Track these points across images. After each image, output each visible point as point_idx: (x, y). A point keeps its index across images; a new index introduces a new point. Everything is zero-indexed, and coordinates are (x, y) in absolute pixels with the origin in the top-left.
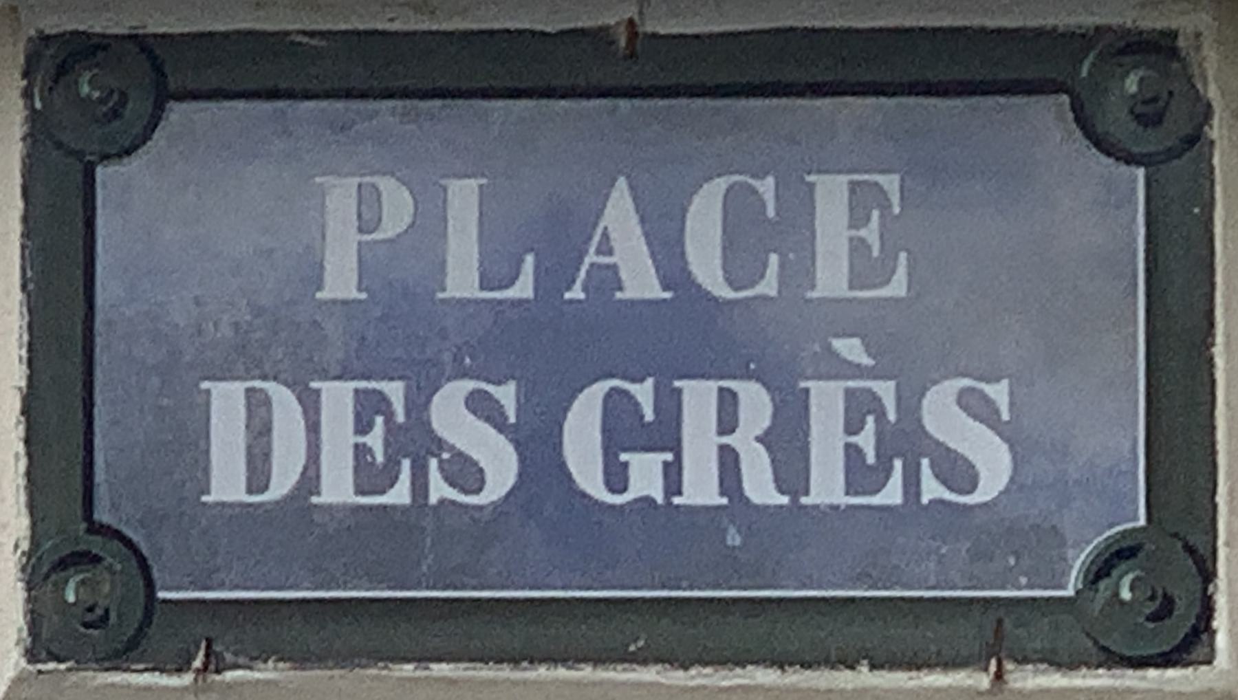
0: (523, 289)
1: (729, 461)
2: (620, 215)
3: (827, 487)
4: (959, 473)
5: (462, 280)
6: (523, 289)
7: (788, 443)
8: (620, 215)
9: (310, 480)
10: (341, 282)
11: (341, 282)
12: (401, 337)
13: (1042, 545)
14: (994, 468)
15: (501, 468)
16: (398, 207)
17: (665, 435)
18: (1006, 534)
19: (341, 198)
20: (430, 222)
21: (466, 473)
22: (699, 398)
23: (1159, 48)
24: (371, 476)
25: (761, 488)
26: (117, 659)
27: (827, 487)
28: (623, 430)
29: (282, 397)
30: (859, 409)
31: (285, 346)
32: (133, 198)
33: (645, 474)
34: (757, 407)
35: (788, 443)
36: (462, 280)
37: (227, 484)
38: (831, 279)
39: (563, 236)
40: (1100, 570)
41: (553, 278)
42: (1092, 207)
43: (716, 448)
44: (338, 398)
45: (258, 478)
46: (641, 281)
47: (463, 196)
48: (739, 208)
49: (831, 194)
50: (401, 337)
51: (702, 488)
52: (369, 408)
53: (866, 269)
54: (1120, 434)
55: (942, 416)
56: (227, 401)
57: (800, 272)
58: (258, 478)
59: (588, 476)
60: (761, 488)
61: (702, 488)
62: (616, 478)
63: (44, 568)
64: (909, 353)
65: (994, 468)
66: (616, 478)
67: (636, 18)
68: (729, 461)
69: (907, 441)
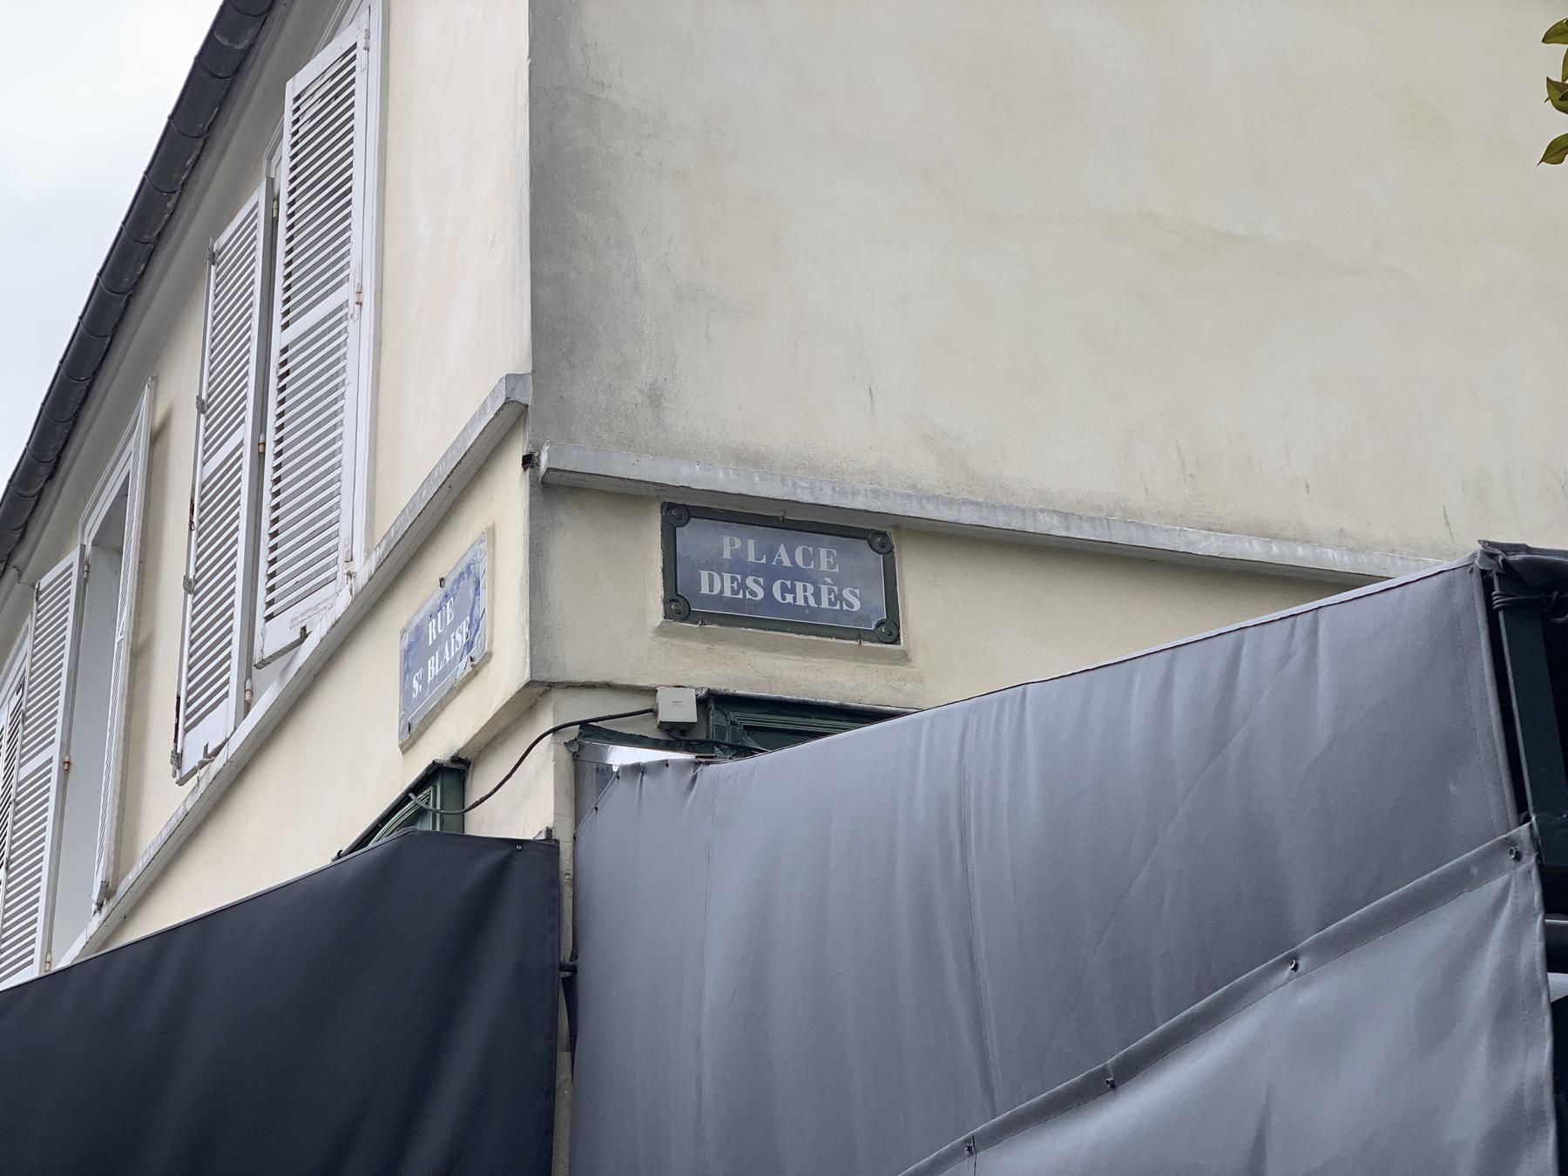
0: (764, 561)
1: (806, 598)
2: (782, 550)
3: (825, 604)
4: (850, 605)
5: (751, 558)
6: (764, 561)
7: (817, 595)
8: (782, 550)
9: (722, 591)
10: (727, 555)
11: (727, 555)
12: (739, 567)
13: (868, 620)
14: (857, 606)
15: (761, 594)
16: (738, 544)
17: (793, 591)
18: (858, 617)
19: (726, 540)
20: (745, 545)
21: (753, 593)
22: (799, 586)
23: (884, 534)
24: (734, 592)
25: (812, 602)
26: (683, 620)
27: (825, 604)
28: (784, 590)
29: (716, 575)
30: (830, 591)
31: (717, 566)
32: (683, 534)
33: (789, 598)
34: (810, 588)
35: (817, 595)
36: (751, 558)
37: (705, 590)
38: (824, 567)
39: (771, 554)
40: (878, 626)
41: (770, 560)
42: (875, 561)
43: (802, 595)
44: (727, 577)
45: (711, 590)
46: (787, 563)
47: (751, 543)
48: (783, 586)
49: (823, 552)
50: (739, 567)
51: (800, 602)
52: (733, 580)
53: (830, 566)
54: (880, 601)
55: (846, 593)
56: (704, 575)
57: (818, 565)
58: (711, 590)
59: (778, 597)
60: (812, 602)
61: (800, 602)
62: (784, 598)
63: (668, 601)
64: (840, 582)
65: (857, 606)
66: (784, 598)
67: (564, 837)
68: (806, 598)
69: (840, 598)
